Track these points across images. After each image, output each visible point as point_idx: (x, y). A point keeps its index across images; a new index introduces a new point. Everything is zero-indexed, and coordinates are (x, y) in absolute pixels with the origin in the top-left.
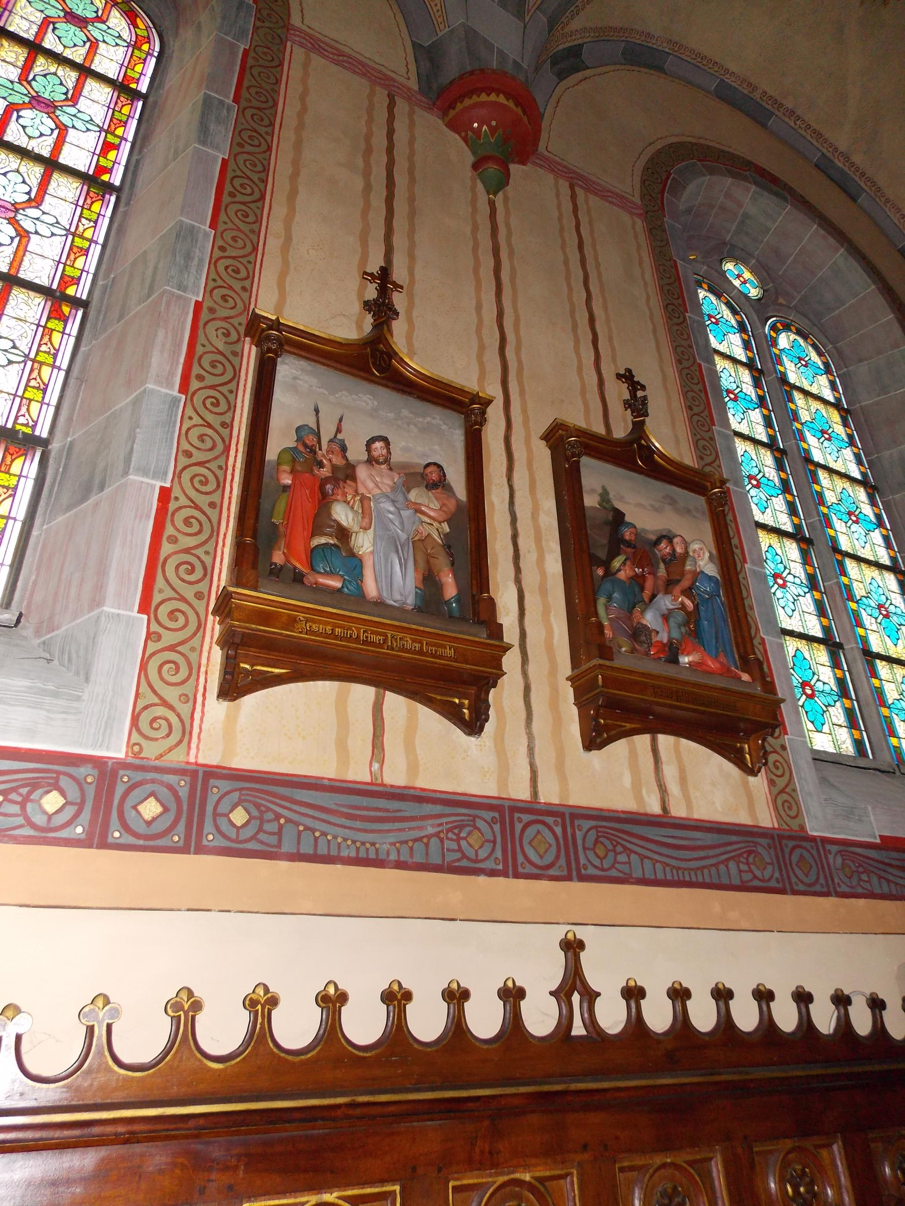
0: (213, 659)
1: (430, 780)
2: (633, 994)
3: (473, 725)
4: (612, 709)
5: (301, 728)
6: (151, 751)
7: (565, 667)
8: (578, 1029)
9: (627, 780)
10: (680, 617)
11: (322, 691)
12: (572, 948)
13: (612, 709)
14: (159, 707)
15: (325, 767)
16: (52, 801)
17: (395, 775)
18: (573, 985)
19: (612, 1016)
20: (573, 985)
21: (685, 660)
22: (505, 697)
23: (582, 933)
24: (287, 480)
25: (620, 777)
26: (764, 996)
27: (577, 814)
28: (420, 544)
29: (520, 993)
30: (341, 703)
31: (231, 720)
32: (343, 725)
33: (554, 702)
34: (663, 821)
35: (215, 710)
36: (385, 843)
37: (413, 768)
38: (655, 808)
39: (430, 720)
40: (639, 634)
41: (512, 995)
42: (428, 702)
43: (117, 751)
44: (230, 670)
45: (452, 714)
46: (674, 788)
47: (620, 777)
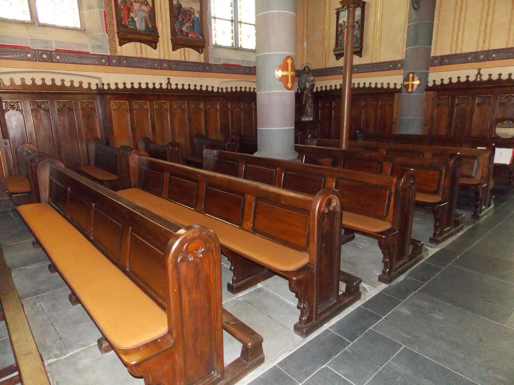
0: (117, 40)
1: (149, 57)
2: (177, 85)
3: (155, 48)
4: (176, 45)
5: (130, 49)
6: (113, 54)
7: (170, 37)
8: (169, 88)
9: (179, 56)
10: (189, 28)
11: (133, 44)
12: (169, 79)
13: (176, 45)
14: (113, 49)
15: (135, 56)
16: (104, 61)
17: (144, 56)
18: (169, 83)
19: (174, 87)
20: (169, 83)
21: (189, 36)
22: (160, 44)
23: (170, 77)
24: (122, 8)
25: (178, 55)
26: (103, 84)
27: (171, 61)
28: (145, 17)
29: (141, 83)
30: (136, 46)
31: (121, 49)
32: (136, 48)
33: (168, 44)
34: (185, 62)
35: (119, 48)
36: (144, 66)
37: (147, 55)
38: (183, 60)
39: (148, 47)
40: (182, 31)
41: (161, 84)
42: (148, 45)
43: (109, 54)
44: (120, 42)
45: (152, 47)
46: (187, 56)
47: (178, 55)
